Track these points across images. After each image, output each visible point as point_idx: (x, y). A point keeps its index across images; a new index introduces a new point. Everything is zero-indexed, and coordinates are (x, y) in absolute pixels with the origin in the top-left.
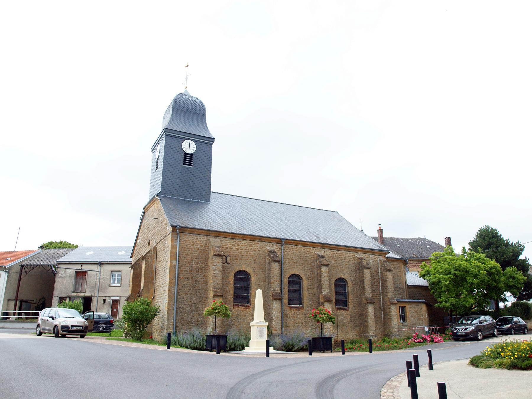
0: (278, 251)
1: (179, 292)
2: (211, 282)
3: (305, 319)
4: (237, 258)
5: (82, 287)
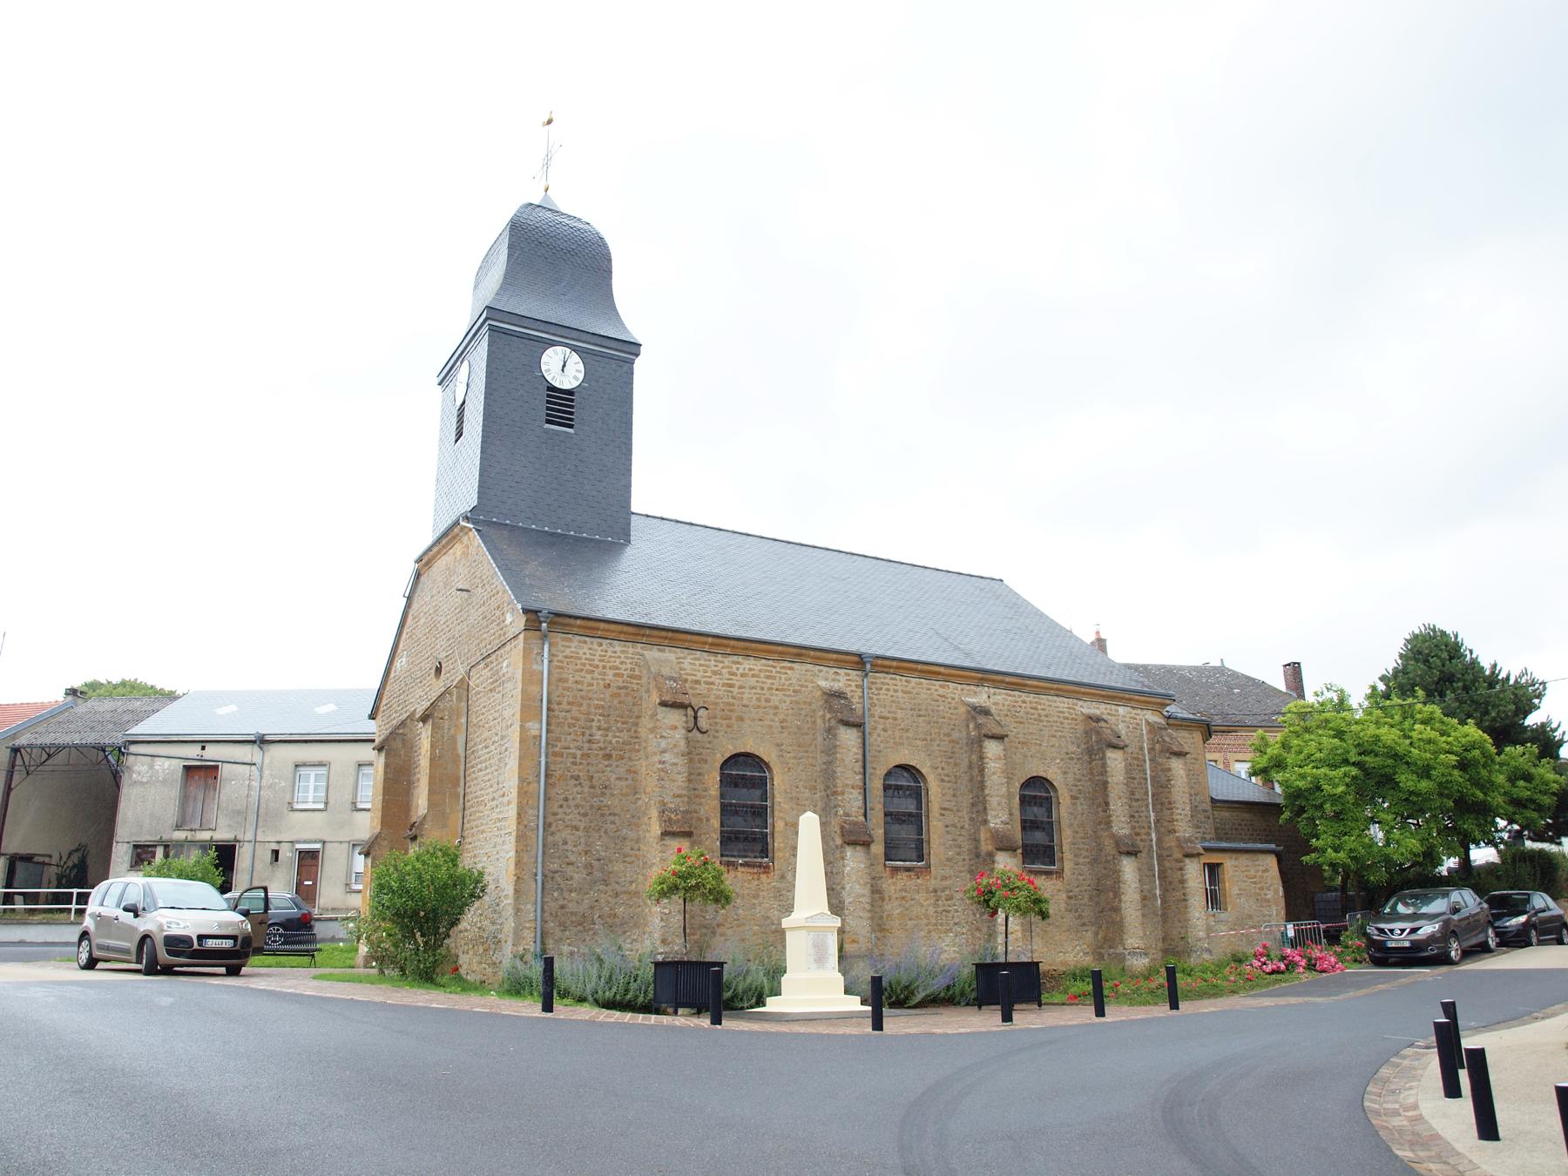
0: (852, 693)
1: (550, 825)
2: (653, 791)
3: (936, 905)
4: (729, 713)
5: (204, 815)
